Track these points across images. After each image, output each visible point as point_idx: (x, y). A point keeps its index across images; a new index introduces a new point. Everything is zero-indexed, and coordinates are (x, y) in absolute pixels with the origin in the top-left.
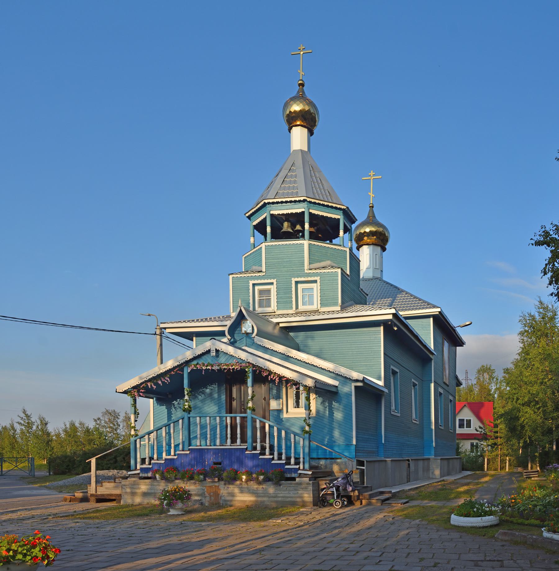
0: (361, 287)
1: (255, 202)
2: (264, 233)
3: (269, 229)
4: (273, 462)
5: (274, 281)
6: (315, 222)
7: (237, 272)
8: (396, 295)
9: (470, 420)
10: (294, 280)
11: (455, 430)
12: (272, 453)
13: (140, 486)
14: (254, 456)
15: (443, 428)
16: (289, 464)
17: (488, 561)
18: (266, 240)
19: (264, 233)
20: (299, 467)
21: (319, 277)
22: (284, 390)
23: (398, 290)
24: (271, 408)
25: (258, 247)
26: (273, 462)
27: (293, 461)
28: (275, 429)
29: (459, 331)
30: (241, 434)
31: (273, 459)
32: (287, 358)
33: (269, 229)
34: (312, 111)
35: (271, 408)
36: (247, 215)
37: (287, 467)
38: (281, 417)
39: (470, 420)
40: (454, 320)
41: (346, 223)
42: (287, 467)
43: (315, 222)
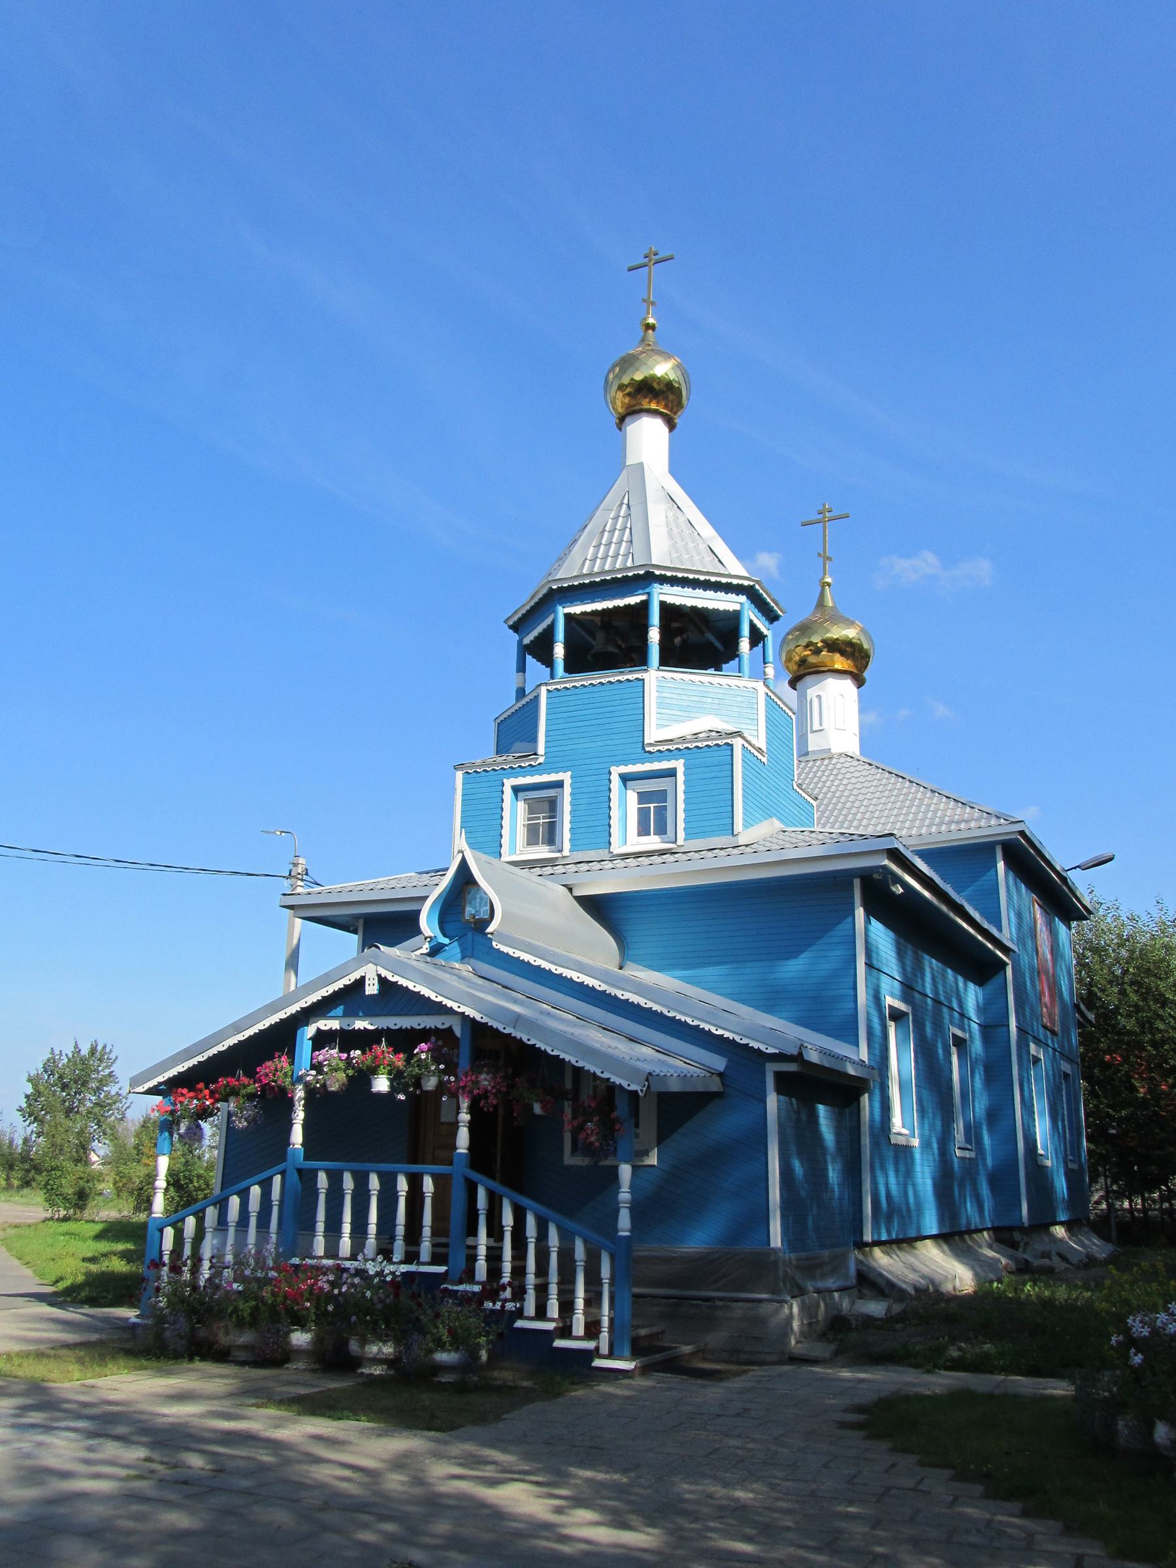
0: (774, 820)
1: (774, 596)
2: (547, 659)
3: (559, 650)
4: (520, 1324)
5: (679, 765)
6: (675, 625)
7: (591, 689)
8: (512, 744)
9: (640, 834)
10: (566, 777)
11: (618, 763)
12: (519, 1293)
13: (774, 1322)
14: (466, 1299)
15: (764, 760)
16: (565, 1331)
17: (822, 594)
18: (552, 677)
19: (547, 659)
20: (597, 1348)
21: (682, 761)
22: (121, 1247)
23: (524, 671)
24: (443, 1120)
25: (531, 697)
26: (520, 1324)
27: (579, 1328)
28: (482, 1194)
29: (1078, 880)
30: (379, 1225)
31: (519, 1314)
32: (964, 1095)
33: (559, 650)
34: (866, 646)
35: (443, 1120)
36: (511, 623)
37: (559, 1343)
38: (113, 1152)
39: (640, 834)
40: (1061, 853)
41: (756, 621)
42: (559, 1343)
43: (675, 625)
